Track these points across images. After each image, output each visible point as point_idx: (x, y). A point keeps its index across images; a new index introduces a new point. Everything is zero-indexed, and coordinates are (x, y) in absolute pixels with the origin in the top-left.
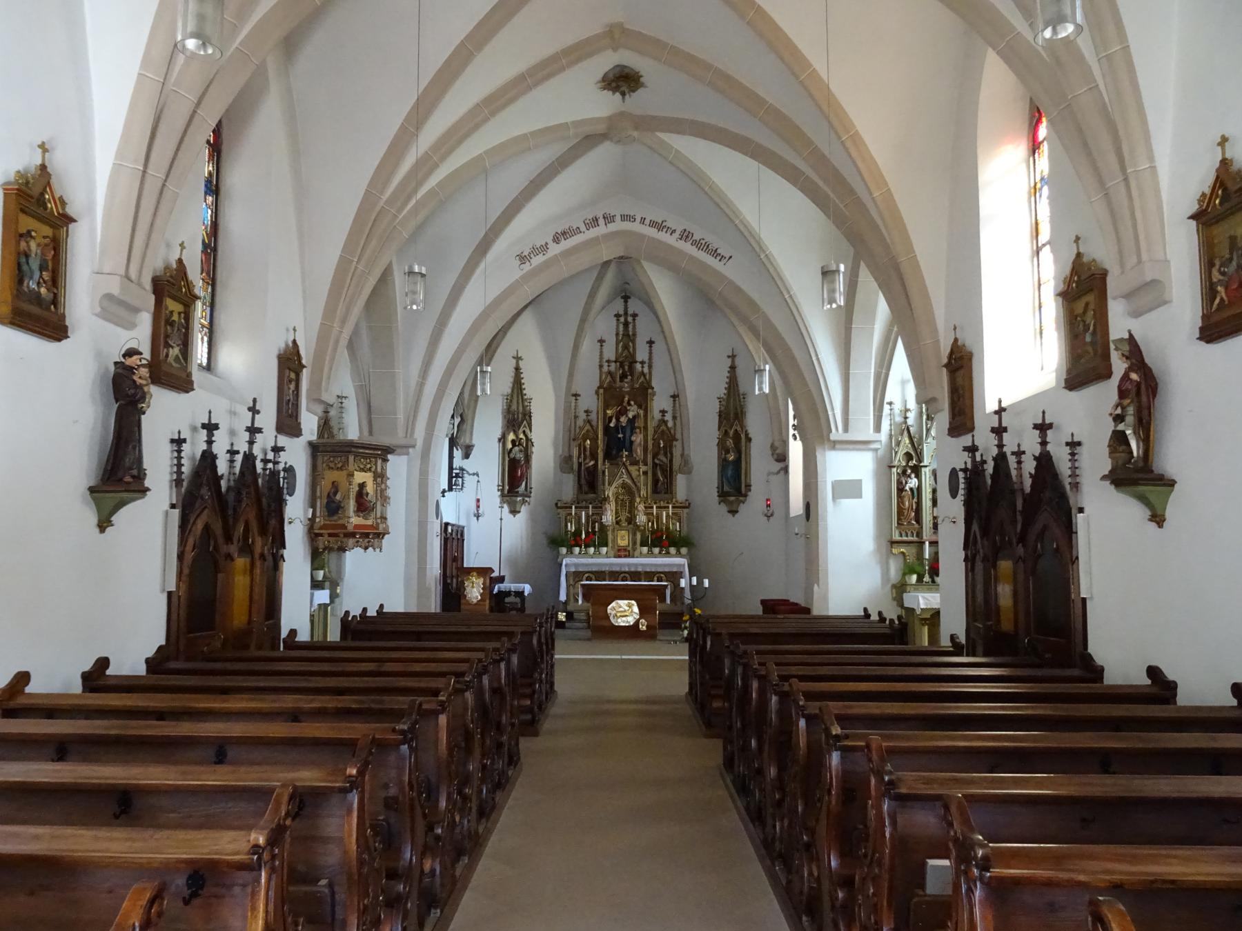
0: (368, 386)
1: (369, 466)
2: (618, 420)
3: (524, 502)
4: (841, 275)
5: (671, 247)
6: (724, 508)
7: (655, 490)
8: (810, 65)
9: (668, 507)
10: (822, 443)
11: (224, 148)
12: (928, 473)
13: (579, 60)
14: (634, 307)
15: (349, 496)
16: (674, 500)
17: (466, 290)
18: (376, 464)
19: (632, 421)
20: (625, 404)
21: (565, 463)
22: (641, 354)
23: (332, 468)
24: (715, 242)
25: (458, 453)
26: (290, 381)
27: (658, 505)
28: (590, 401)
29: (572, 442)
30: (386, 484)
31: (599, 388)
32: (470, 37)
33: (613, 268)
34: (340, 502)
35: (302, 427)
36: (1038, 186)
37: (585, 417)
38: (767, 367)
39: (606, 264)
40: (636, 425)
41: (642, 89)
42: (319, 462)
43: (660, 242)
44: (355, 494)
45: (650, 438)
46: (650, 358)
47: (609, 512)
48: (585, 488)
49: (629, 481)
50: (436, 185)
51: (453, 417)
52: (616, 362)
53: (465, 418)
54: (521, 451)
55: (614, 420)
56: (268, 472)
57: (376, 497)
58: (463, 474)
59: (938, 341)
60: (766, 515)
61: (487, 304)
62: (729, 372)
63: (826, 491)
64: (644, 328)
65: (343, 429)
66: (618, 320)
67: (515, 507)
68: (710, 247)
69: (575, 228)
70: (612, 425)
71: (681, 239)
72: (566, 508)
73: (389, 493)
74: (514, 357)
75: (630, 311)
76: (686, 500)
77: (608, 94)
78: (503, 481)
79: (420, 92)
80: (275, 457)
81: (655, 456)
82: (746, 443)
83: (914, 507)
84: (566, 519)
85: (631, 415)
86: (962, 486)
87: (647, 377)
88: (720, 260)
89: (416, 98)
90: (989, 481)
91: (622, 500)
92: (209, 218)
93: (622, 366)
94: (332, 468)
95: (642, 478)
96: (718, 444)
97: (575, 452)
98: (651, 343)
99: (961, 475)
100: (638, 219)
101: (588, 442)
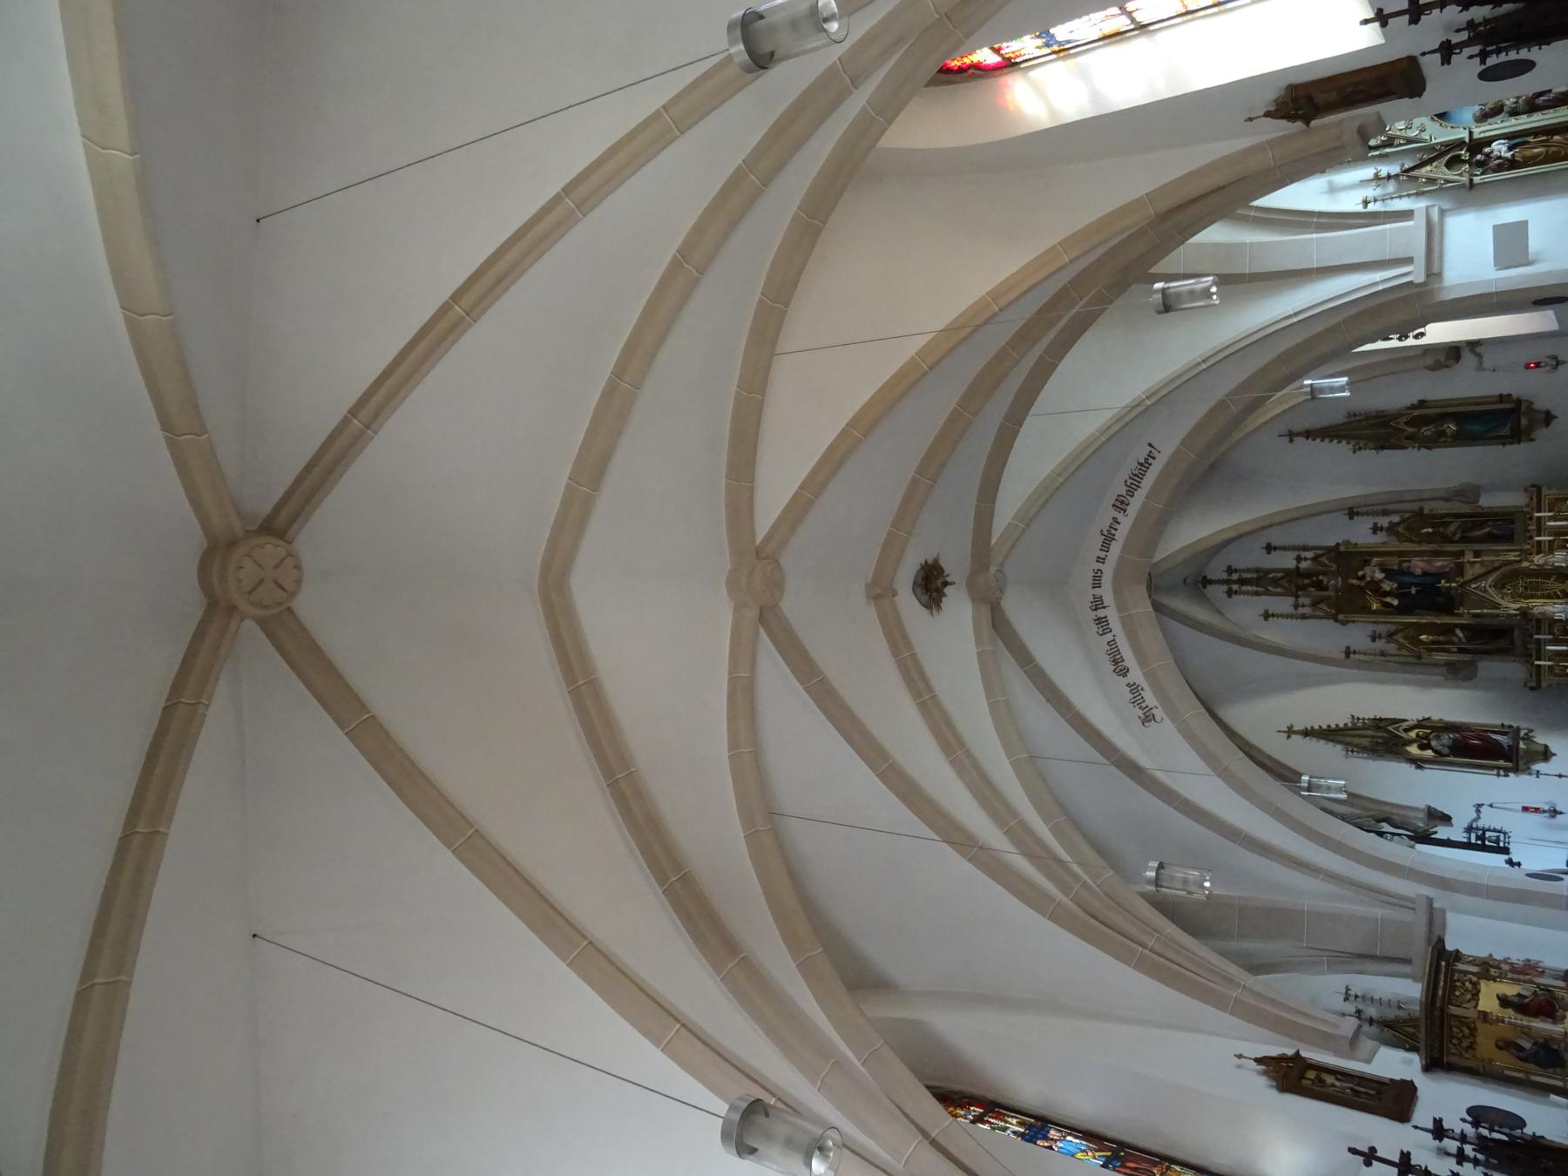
0: (1328, 953)
1: (1467, 984)
2: (1387, 594)
3: (1528, 738)
4: (1171, 285)
5: (1134, 525)
6: (1541, 433)
7: (1508, 538)
8: (913, 358)
9: (1539, 518)
10: (1431, 293)
11: (991, 1096)
12: (1483, 129)
13: (905, 637)
14: (1216, 571)
15: (1522, 1027)
16: (1525, 510)
17: (1190, 798)
18: (1466, 973)
19: (1390, 574)
20: (1363, 584)
21: (1459, 673)
22: (1287, 561)
23: (1472, 1043)
24: (1130, 465)
25: (1442, 832)
26: (1322, 1081)
27: (1535, 533)
28: (1357, 634)
29: (1423, 661)
30: (1500, 962)
31: (1337, 621)
32: (873, 767)
33: (1167, 600)
34: (1535, 1044)
35: (1397, 1078)
36: (1056, 48)
37: (1383, 641)
38: (1308, 382)
39: (1158, 607)
40: (1396, 568)
41: (940, 562)
42: (1455, 1060)
43: (1128, 538)
44: (1520, 1016)
45: (1418, 548)
46: (1294, 548)
47: (1545, 608)
48: (1502, 643)
49: (1491, 579)
50: (1047, 825)
51: (1381, 834)
52: (1297, 597)
53: (1382, 816)
54: (1438, 737)
55: (1388, 600)
56: (1480, 1156)
57: (1525, 982)
58: (1477, 829)
59: (1269, 142)
60: (1556, 367)
61: (1210, 771)
62: (1314, 439)
63: (1516, 276)
64: (1251, 558)
65: (1399, 1001)
66: (1236, 592)
67: (1537, 752)
68: (1136, 472)
69: (1108, 648)
70: (1396, 602)
71: (1125, 511)
72: (1538, 674)
73: (1517, 957)
74: (1289, 737)
75: (1225, 576)
76: (1526, 490)
77: (945, 602)
78: (1492, 768)
79: (937, 838)
80: (1454, 1138)
81: (1447, 539)
82: (1428, 407)
83: (1545, 138)
84: (1559, 675)
85: (1379, 575)
86: (1513, 55)
87: (1320, 552)
88: (1154, 458)
89: (945, 844)
90: (1507, 7)
91: (1526, 588)
92: (1078, 1141)
93: (1303, 588)
94: (1472, 1043)
95: (1486, 559)
96: (1429, 448)
97: (1441, 657)
98: (1269, 548)
99: (1492, 61)
100: (1100, 566)
101: (1423, 637)
